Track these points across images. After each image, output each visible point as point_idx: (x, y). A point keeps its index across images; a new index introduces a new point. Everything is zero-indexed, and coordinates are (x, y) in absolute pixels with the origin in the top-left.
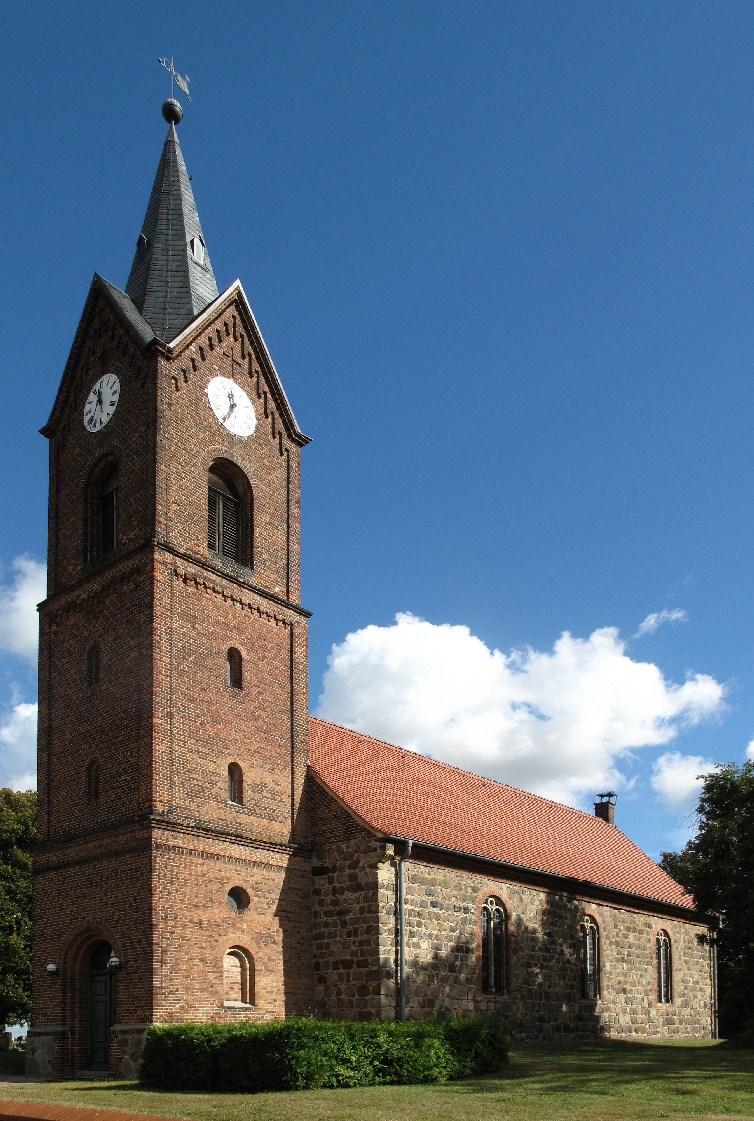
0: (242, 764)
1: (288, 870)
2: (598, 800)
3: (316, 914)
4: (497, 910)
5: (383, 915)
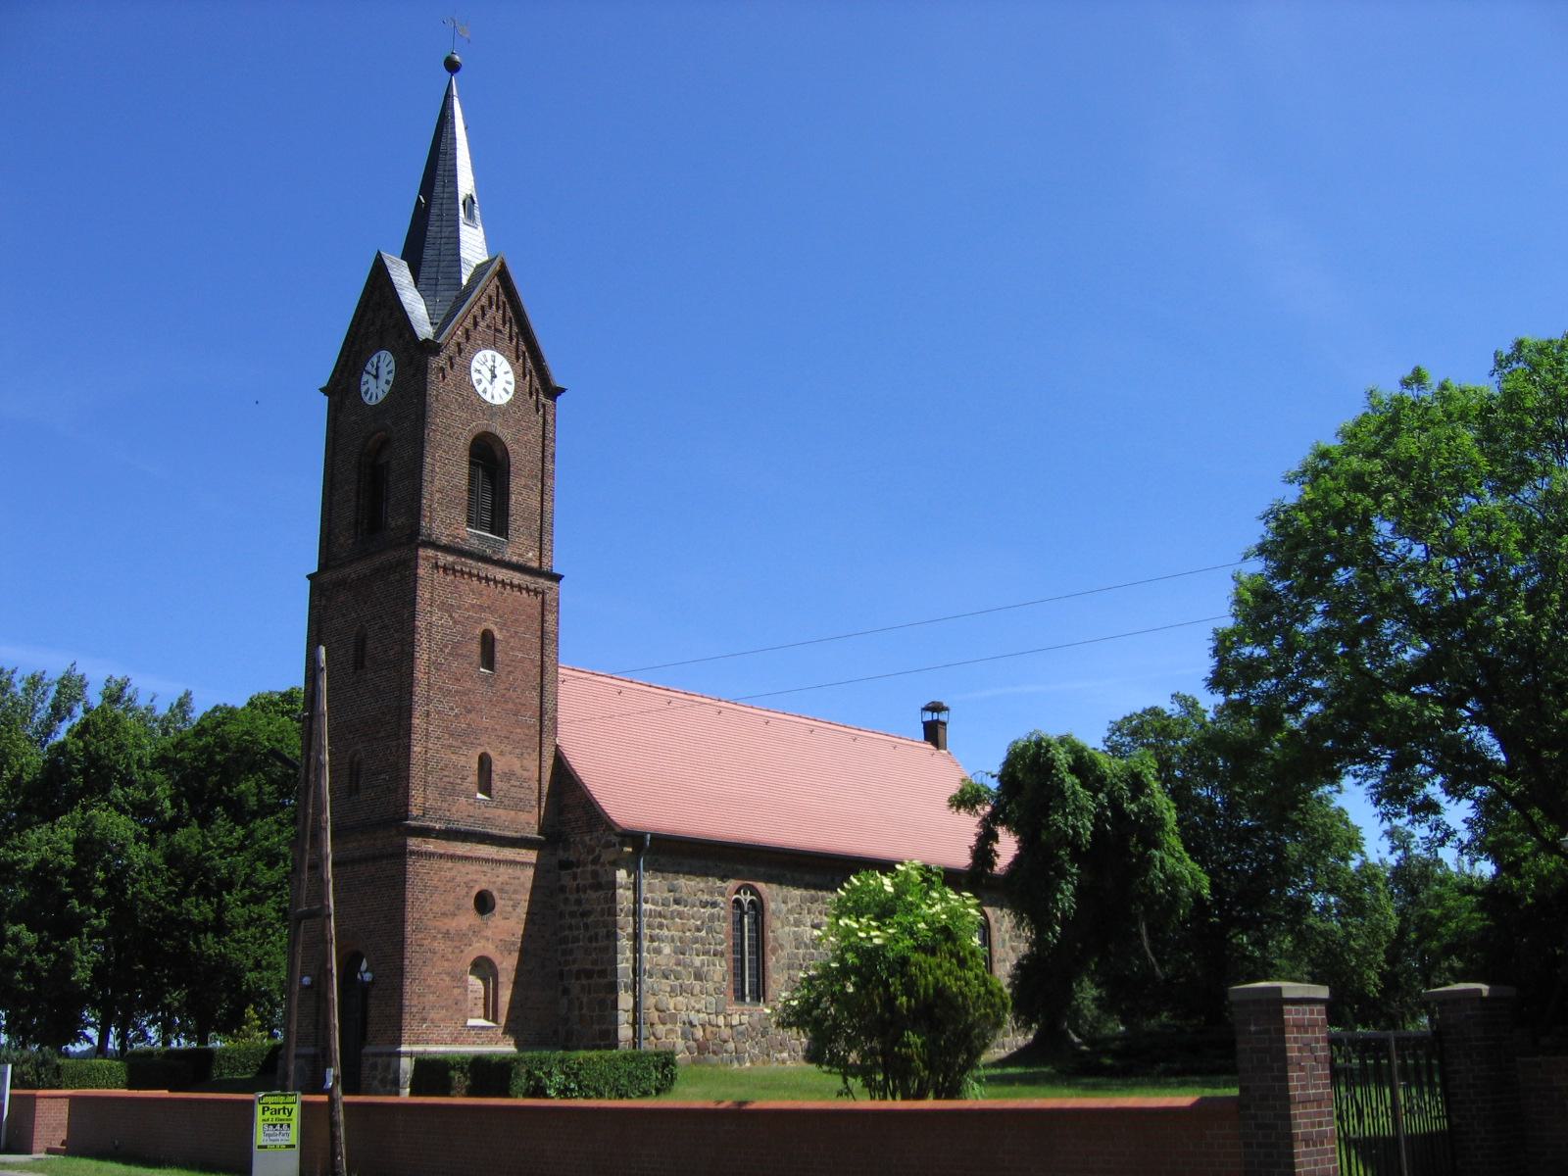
1: (537, 867)
2: (928, 717)
3: (562, 915)
5: (621, 919)
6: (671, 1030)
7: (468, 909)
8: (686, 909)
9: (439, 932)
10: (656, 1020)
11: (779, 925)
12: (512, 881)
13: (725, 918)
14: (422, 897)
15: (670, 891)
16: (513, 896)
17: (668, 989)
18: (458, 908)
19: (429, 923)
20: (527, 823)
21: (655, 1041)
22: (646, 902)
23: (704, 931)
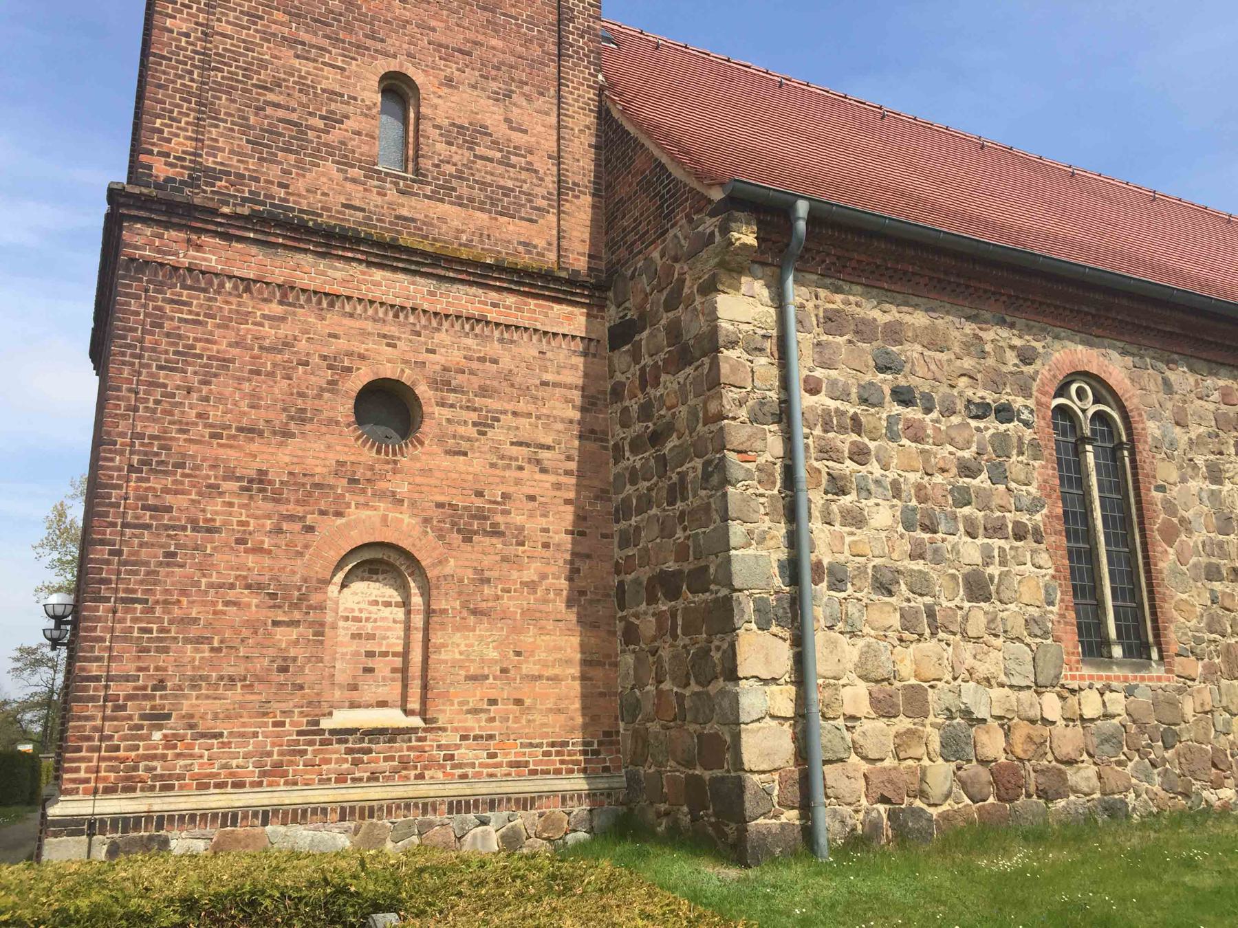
0: (419, 78)
4: (1100, 417)
6: (910, 732)
7: (332, 422)
8: (928, 418)
9: (231, 476)
10: (864, 708)
11: (1174, 476)
12: (475, 365)
13: (1034, 445)
14: (173, 381)
15: (881, 369)
16: (478, 402)
17: (895, 620)
18: (301, 417)
19: (192, 449)
20: (526, 244)
21: (865, 767)
22: (813, 390)
23: (984, 476)
